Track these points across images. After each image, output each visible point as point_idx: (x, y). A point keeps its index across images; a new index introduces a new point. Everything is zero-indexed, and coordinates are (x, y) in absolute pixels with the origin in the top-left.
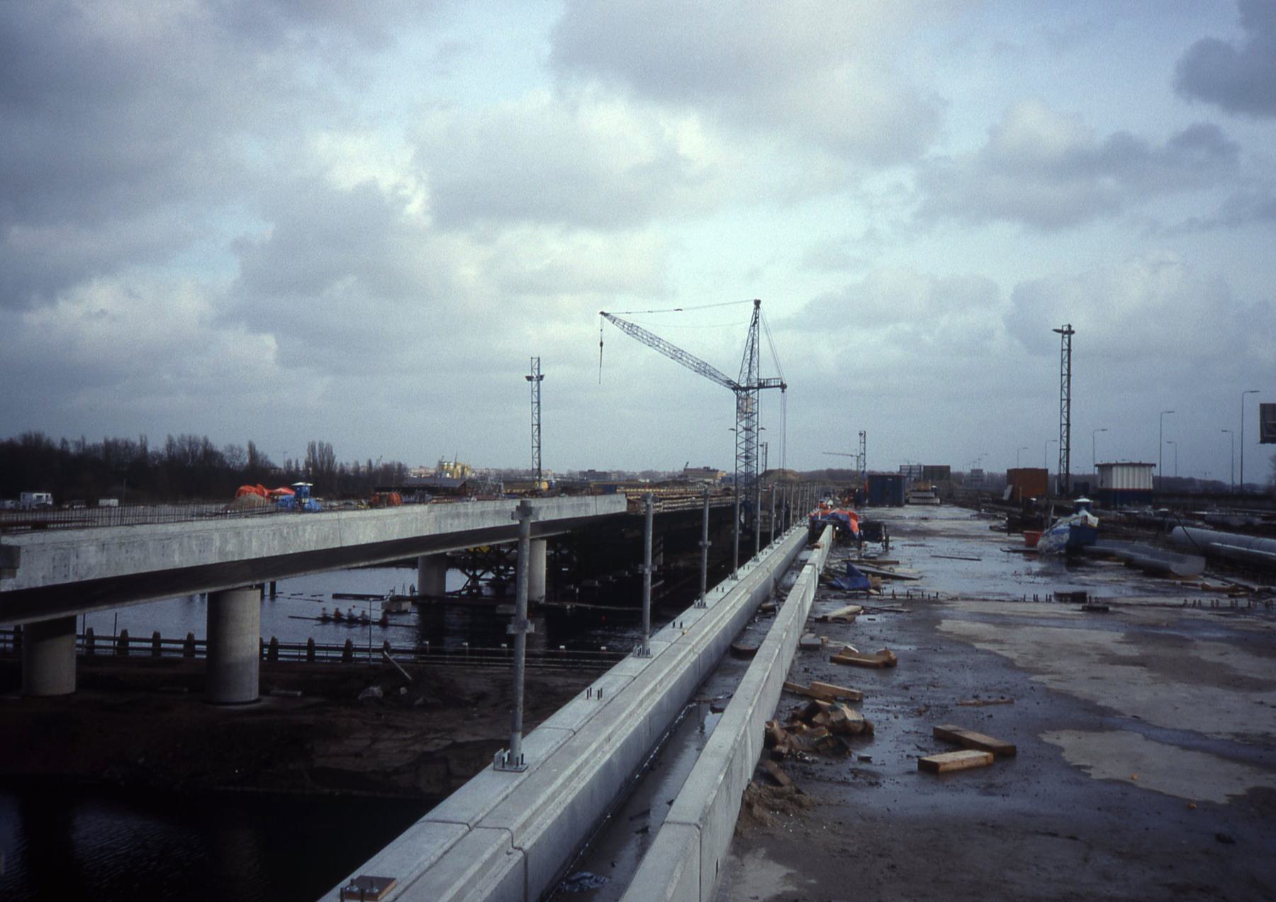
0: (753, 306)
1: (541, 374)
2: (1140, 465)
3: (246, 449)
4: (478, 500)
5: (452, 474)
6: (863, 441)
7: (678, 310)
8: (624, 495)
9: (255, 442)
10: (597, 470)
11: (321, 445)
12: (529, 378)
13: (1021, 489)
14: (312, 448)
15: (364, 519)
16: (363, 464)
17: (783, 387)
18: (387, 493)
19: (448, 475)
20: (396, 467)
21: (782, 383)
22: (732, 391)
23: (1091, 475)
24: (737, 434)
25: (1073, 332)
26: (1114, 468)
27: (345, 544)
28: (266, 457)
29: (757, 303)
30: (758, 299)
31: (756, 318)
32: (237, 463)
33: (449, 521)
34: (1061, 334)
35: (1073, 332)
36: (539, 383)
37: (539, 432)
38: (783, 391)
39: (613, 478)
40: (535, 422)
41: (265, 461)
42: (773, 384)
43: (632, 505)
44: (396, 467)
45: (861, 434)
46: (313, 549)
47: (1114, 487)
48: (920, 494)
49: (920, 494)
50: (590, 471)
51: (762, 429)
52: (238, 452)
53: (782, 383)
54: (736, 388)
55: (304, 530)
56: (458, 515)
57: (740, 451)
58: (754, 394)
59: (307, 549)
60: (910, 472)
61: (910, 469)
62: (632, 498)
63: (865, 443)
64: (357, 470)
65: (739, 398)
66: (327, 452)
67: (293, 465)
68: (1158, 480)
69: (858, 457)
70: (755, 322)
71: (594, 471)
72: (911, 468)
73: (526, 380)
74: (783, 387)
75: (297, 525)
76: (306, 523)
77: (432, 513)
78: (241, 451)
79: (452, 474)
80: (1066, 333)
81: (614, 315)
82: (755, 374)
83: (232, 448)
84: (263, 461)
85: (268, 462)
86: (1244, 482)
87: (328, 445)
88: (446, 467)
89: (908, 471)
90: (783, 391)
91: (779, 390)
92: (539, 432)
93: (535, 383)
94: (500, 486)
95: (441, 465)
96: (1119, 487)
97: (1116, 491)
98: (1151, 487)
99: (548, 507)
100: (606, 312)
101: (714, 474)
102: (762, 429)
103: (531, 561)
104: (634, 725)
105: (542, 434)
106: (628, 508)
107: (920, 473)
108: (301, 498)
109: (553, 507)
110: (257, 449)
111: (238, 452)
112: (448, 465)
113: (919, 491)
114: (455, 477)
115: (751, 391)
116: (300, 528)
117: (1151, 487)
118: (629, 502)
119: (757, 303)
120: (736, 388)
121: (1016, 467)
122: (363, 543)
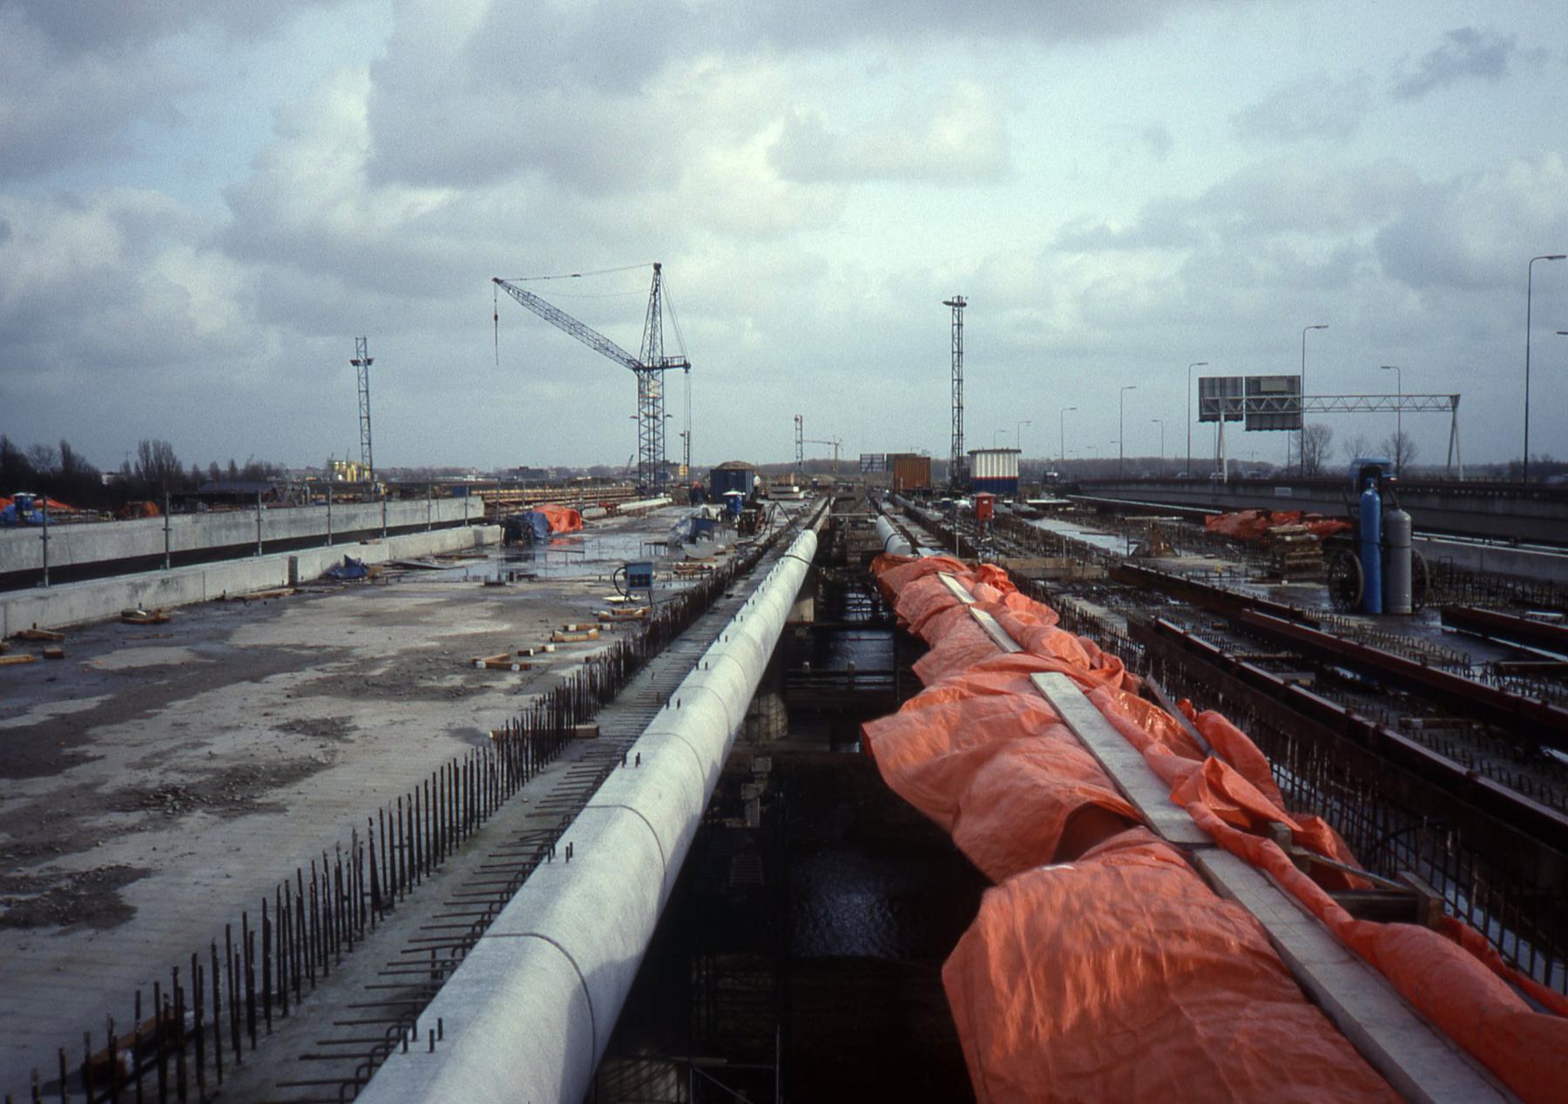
0: (653, 270)
1: (369, 357)
2: (1008, 451)
3: (58, 449)
4: (268, 508)
5: (345, 475)
6: (799, 427)
7: (575, 276)
8: (480, 498)
9: (69, 442)
10: (530, 468)
11: (156, 445)
12: (355, 363)
13: (902, 480)
14: (145, 448)
15: (105, 532)
16: (204, 468)
17: (686, 366)
18: (140, 503)
19: (340, 477)
20: (264, 469)
21: (685, 362)
22: (632, 372)
23: (1114, 461)
24: (640, 423)
25: (965, 305)
26: (978, 456)
27: (77, 561)
28: (83, 460)
29: (658, 267)
30: (658, 262)
31: (657, 285)
32: (47, 469)
33: (224, 533)
34: (951, 307)
35: (965, 305)
36: (366, 368)
37: (369, 426)
38: (687, 372)
39: (551, 476)
40: (364, 415)
41: (83, 464)
42: (676, 363)
43: (489, 510)
44: (264, 469)
45: (796, 420)
46: (33, 567)
47: (978, 475)
48: (779, 489)
49: (779, 489)
50: (521, 468)
51: (669, 416)
52: (47, 455)
53: (685, 362)
54: (638, 368)
55: (19, 548)
56: (236, 526)
57: (644, 443)
58: (659, 375)
59: (25, 567)
60: (872, 463)
61: (872, 459)
62: (489, 501)
63: (801, 429)
64: (197, 474)
65: (641, 381)
66: (164, 452)
67: (133, 470)
68: (1023, 468)
69: (837, 445)
70: (656, 290)
71: (527, 468)
72: (872, 457)
73: (351, 364)
74: (686, 366)
75: (10, 542)
76: (23, 539)
77: (198, 525)
78: (51, 453)
79: (345, 475)
80: (956, 305)
81: (510, 282)
82: (658, 351)
83: (39, 450)
84: (80, 466)
85: (87, 466)
86: (1530, 459)
87: (166, 443)
88: (337, 467)
89: (869, 461)
90: (687, 372)
91: (682, 370)
92: (369, 426)
93: (361, 368)
94: (306, 491)
95: (331, 465)
96: (983, 475)
97: (981, 479)
98: (1017, 475)
99: (367, 514)
100: (500, 278)
101: (675, 468)
102: (669, 416)
103: (1467, 635)
104: (1118, 859)
105: (372, 428)
106: (485, 514)
107: (883, 463)
108: (22, 510)
109: (374, 514)
110: (72, 450)
111: (47, 455)
112: (340, 465)
113: (780, 485)
114: (349, 479)
115: (655, 372)
116: (14, 545)
117: (1017, 475)
118: (487, 505)
119: (658, 267)
120: (638, 368)
121: (1157, 455)
122: (102, 559)
